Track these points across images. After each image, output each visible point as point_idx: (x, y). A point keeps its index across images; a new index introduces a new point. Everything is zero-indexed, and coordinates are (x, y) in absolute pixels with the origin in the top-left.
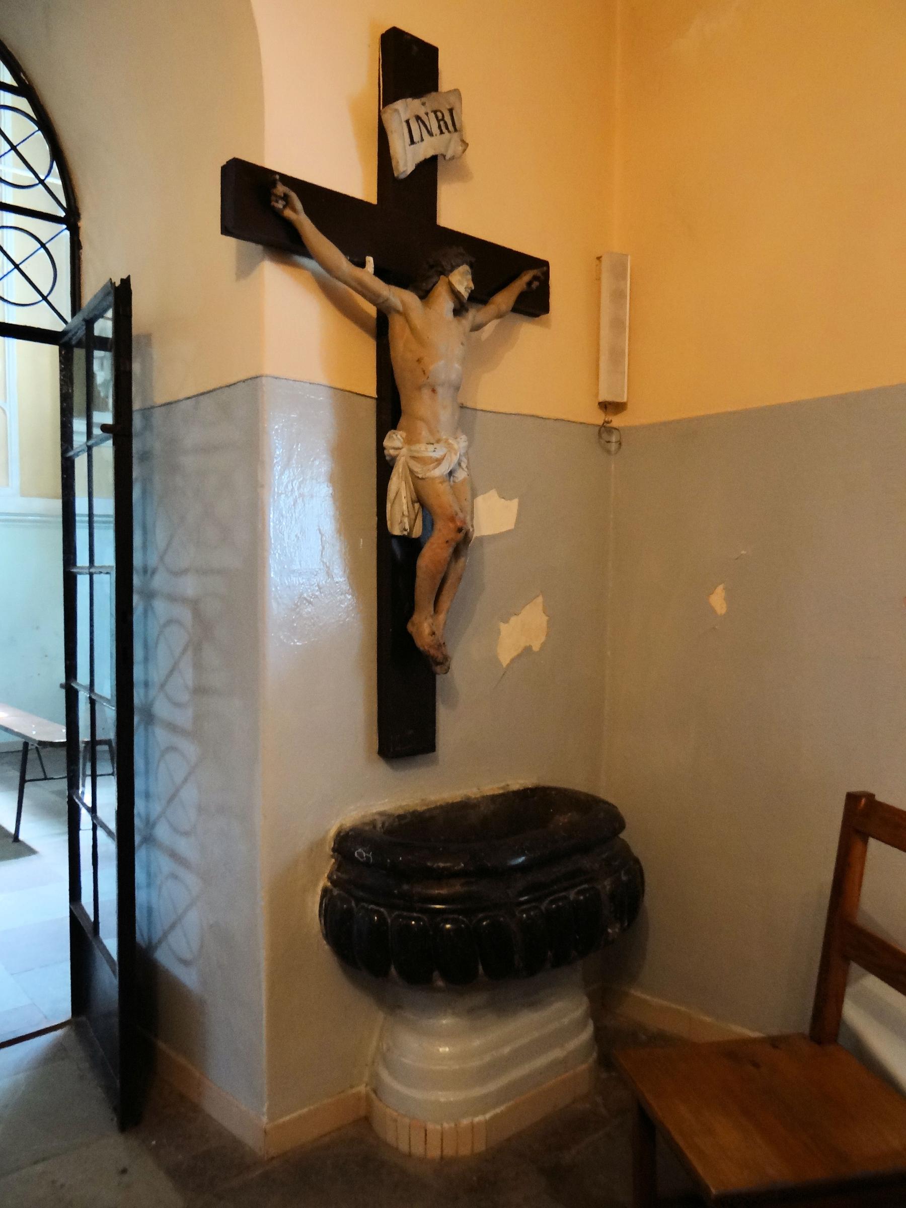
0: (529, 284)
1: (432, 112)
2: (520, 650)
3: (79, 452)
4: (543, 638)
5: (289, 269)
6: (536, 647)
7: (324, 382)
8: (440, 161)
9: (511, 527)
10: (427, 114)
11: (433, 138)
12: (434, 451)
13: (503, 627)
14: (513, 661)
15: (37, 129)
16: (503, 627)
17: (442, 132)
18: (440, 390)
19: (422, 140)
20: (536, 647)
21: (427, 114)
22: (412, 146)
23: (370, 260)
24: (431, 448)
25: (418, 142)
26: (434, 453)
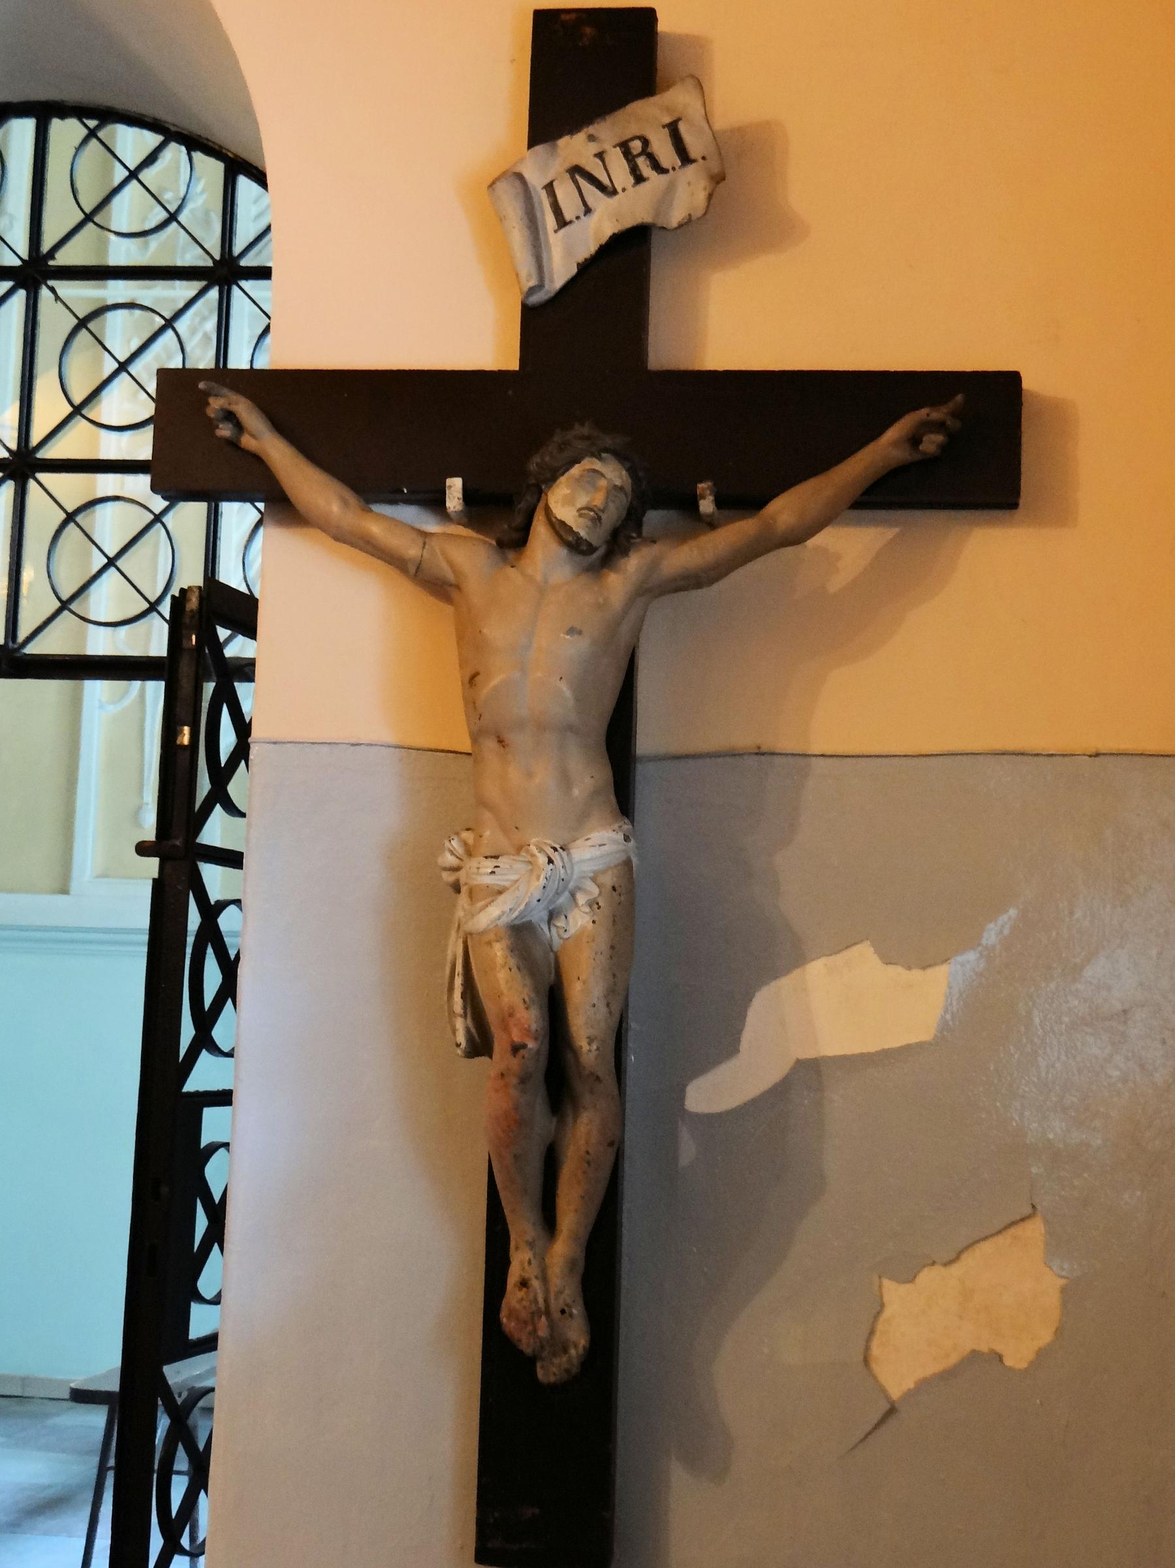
0: (914, 440)
1: (615, 147)
2: (954, 1359)
3: (544, 851)
4: (1045, 1336)
5: (305, 530)
6: (1018, 1356)
7: (389, 737)
8: (656, 239)
9: (924, 1034)
10: (600, 156)
11: (617, 198)
12: (493, 872)
13: (894, 1293)
14: (924, 1385)
15: (188, 366)
16: (894, 1293)
17: (639, 179)
18: (511, 737)
19: (588, 210)
20: (1018, 1356)
21: (600, 156)
22: (563, 231)
23: (455, 486)
24: (489, 865)
25: (578, 218)
26: (493, 876)
